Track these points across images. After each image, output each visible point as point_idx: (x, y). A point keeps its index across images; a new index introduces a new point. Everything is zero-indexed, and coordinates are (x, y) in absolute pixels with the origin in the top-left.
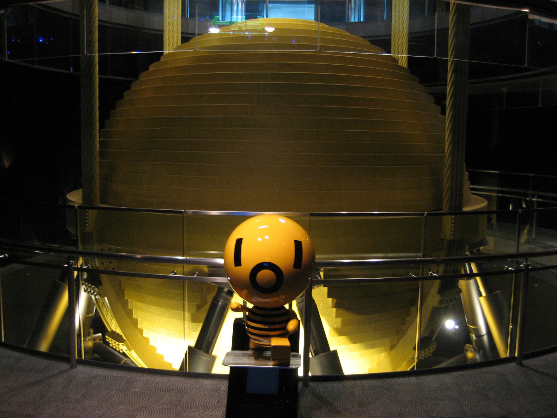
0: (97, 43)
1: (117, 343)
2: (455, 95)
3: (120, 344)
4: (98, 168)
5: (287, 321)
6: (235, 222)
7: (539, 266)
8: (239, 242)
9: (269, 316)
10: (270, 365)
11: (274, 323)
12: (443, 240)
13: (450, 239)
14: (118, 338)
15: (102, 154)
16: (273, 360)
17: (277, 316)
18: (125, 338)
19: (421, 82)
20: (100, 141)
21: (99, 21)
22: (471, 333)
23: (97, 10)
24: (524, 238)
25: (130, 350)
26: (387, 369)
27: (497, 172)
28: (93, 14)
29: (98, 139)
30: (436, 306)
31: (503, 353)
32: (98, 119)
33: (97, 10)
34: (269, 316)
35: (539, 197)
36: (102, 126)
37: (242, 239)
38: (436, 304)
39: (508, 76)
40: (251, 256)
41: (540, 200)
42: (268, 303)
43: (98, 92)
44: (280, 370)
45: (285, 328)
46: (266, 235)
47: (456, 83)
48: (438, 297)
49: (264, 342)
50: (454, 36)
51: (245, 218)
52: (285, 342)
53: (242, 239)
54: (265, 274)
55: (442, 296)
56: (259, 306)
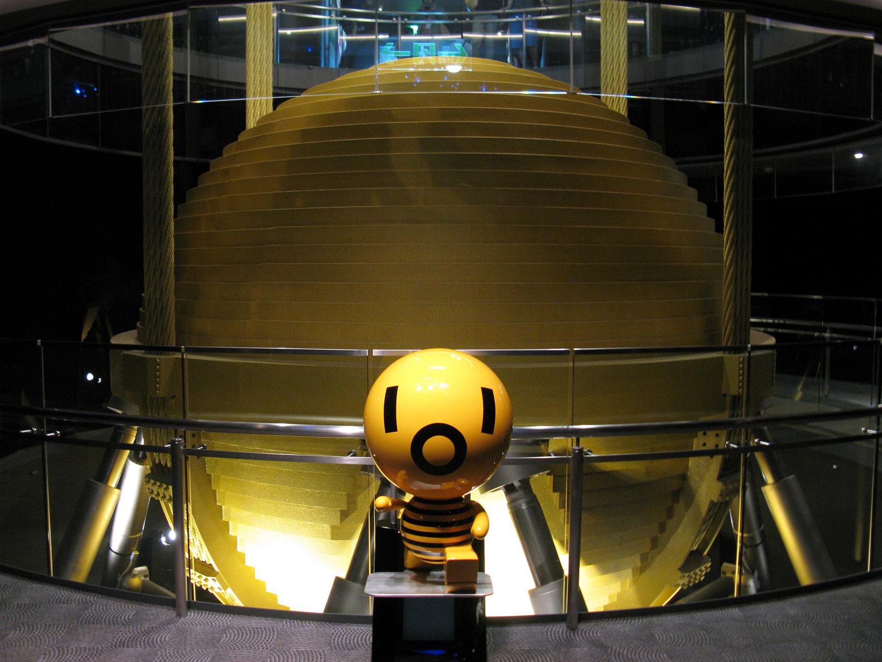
0: (171, 93)
1: (204, 577)
2: (736, 170)
3: (210, 578)
4: (172, 294)
5: (471, 520)
6: (384, 363)
7: (834, 437)
8: (392, 393)
9: (446, 513)
10: (443, 591)
11: (451, 524)
12: (725, 396)
13: (736, 394)
14: (206, 569)
15: (178, 272)
16: (449, 584)
17: (454, 512)
18: (216, 569)
19: (668, 152)
20: (175, 162)
21: (174, 74)
22: (520, 487)
23: (171, 59)
24: (799, 396)
25: (225, 588)
26: (633, 604)
27: (766, 295)
28: (166, 141)
29: (171, 157)
30: (716, 500)
31: (804, 575)
32: (171, 34)
33: (171, 59)
34: (446, 513)
35: (833, 331)
36: (179, 198)
37: (396, 387)
38: (715, 498)
39: (813, 142)
40: (412, 418)
41: (834, 335)
42: (434, 491)
43: (172, 192)
44: (456, 599)
45: (468, 531)
46: (438, 384)
47: (736, 151)
48: (719, 486)
49: (433, 556)
50: (733, 79)
51: (392, 359)
52: (466, 553)
53: (396, 387)
54: (438, 444)
55: (725, 484)
56: (425, 496)
